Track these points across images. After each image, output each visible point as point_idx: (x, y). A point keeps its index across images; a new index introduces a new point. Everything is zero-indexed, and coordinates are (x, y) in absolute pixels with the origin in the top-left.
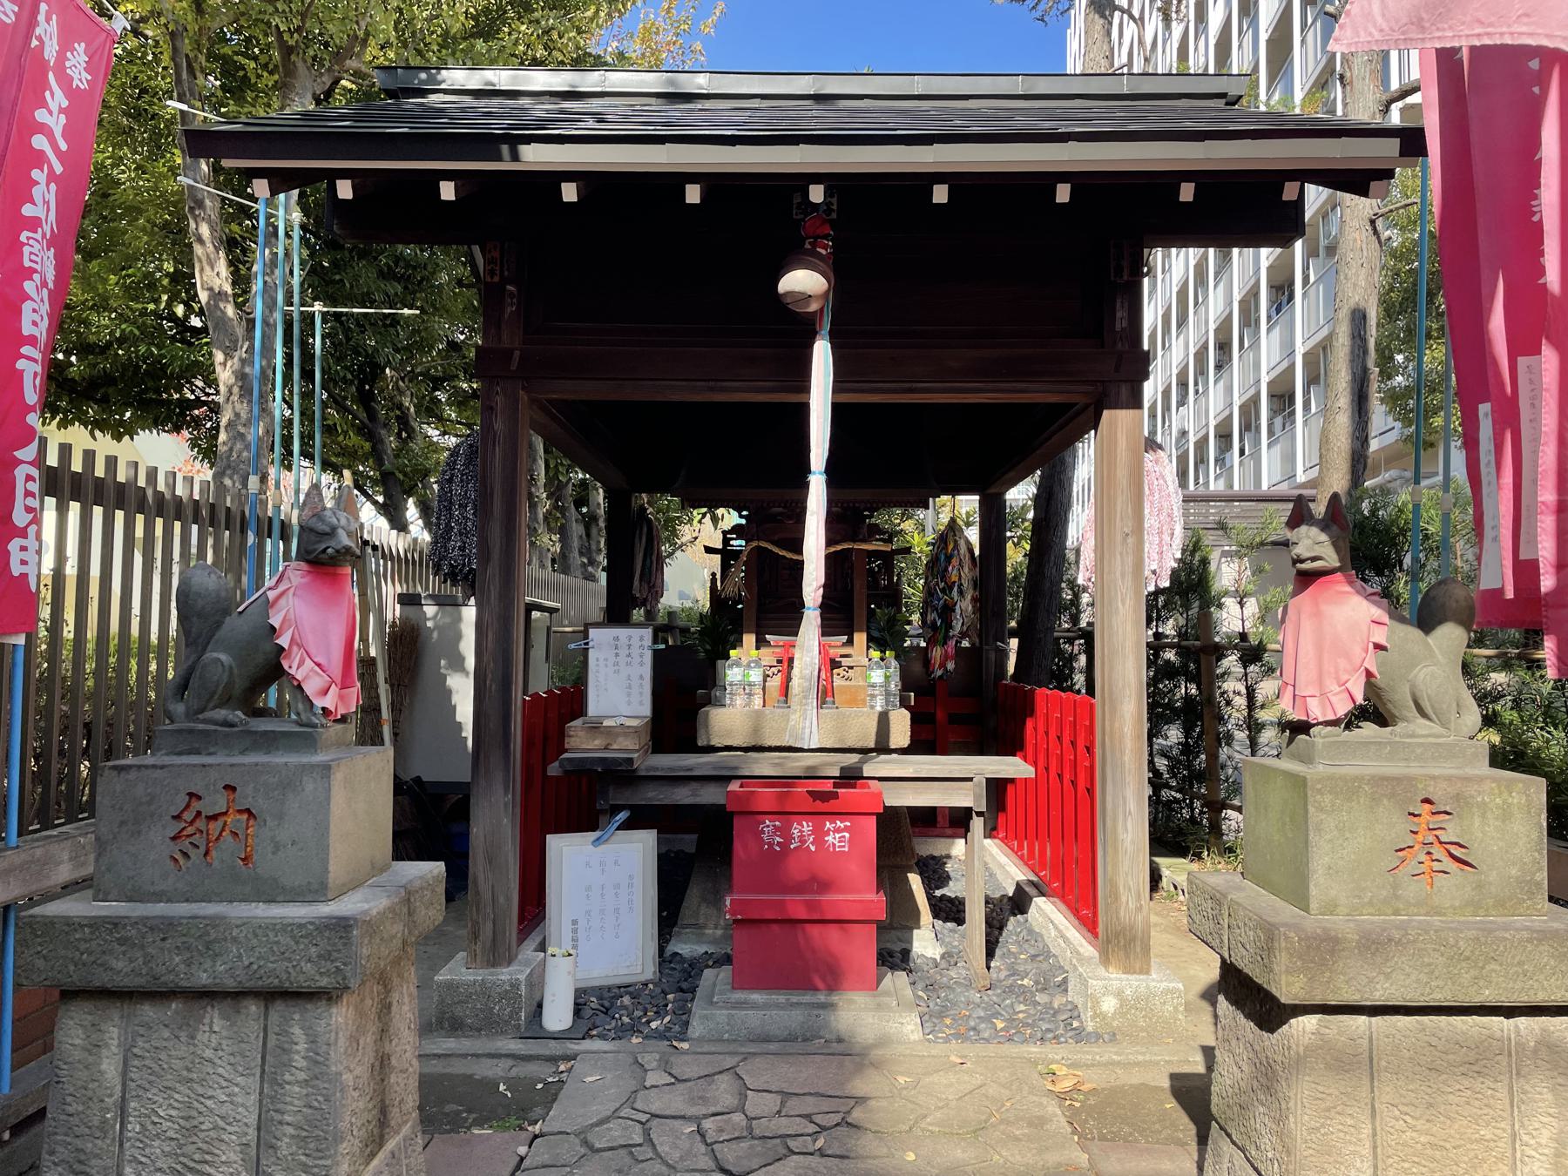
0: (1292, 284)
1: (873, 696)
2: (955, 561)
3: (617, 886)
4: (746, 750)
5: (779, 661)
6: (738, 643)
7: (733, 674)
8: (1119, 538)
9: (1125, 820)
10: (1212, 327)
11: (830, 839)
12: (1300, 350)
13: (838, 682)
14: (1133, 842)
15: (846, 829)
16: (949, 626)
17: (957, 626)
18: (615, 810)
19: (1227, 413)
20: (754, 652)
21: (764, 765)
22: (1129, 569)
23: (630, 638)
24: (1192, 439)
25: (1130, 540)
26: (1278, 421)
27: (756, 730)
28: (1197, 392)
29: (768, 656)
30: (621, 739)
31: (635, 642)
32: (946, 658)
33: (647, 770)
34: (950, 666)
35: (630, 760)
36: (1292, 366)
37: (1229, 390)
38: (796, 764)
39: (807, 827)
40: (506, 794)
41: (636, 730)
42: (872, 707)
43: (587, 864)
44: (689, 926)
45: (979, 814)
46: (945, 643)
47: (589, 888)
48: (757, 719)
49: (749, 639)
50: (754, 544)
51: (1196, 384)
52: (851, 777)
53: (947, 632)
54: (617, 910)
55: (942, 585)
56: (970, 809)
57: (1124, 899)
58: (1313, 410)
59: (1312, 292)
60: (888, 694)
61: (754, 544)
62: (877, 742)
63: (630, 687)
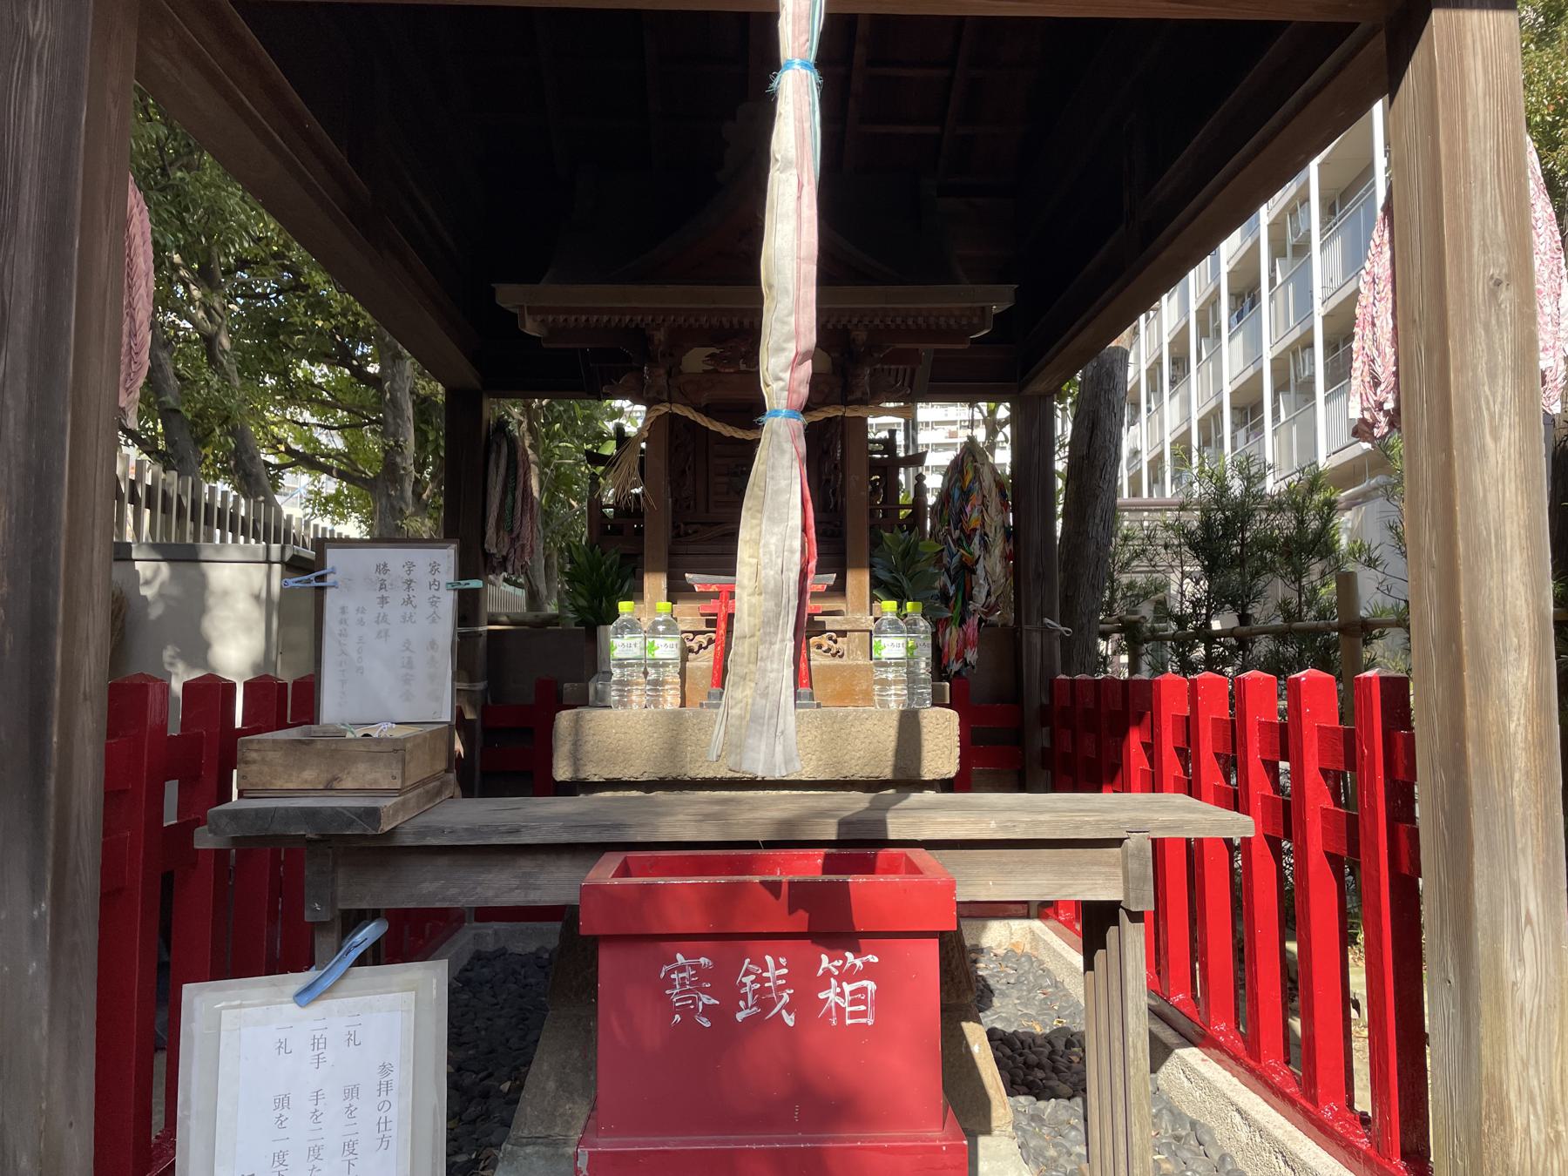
0: (1257, 284)
1: (885, 683)
2: (975, 499)
3: (352, 1092)
4: (648, 786)
5: (709, 623)
6: (636, 594)
7: (621, 646)
8: (1480, 289)
9: (1518, 932)
10: (1166, 340)
11: (830, 995)
12: (1319, 311)
13: (818, 660)
14: (1537, 989)
15: (868, 972)
16: (968, 597)
17: (980, 594)
18: (353, 920)
19: (1184, 428)
20: (664, 606)
21: (683, 820)
22: (1505, 359)
23: (410, 566)
24: (1145, 458)
25: (1505, 295)
26: (1242, 433)
27: (673, 746)
28: (1149, 410)
29: (690, 615)
30: (362, 767)
31: (421, 573)
32: (965, 644)
33: (422, 833)
34: (971, 656)
35: (373, 814)
36: (1259, 373)
37: (1186, 402)
38: (759, 815)
39: (775, 969)
40: (35, 902)
41: (397, 750)
42: (884, 704)
43: (282, 1046)
44: (533, 1140)
45: (1136, 917)
46: (963, 621)
47: (283, 1101)
48: (675, 731)
49: (655, 584)
50: (663, 409)
51: (1148, 401)
52: (861, 846)
53: (965, 604)
54: (350, 1147)
55: (956, 534)
56: (1115, 905)
57: (1519, 1122)
58: (1283, 418)
59: (1280, 295)
60: (912, 680)
61: (663, 409)
62: (896, 768)
63: (409, 664)
